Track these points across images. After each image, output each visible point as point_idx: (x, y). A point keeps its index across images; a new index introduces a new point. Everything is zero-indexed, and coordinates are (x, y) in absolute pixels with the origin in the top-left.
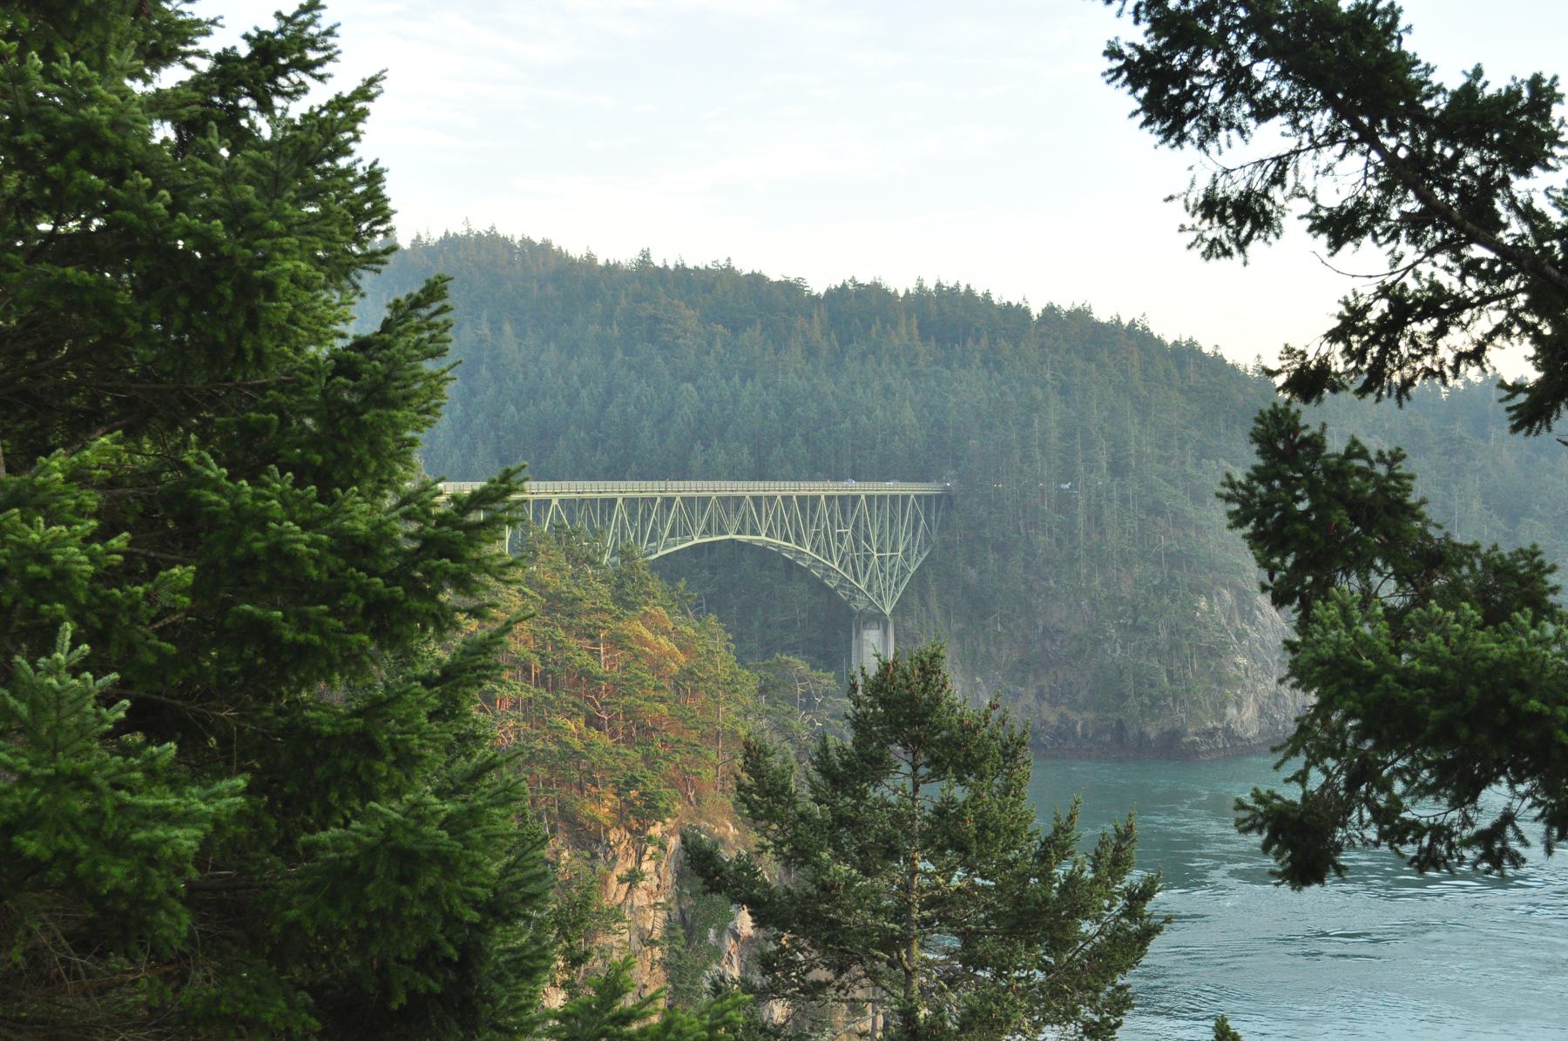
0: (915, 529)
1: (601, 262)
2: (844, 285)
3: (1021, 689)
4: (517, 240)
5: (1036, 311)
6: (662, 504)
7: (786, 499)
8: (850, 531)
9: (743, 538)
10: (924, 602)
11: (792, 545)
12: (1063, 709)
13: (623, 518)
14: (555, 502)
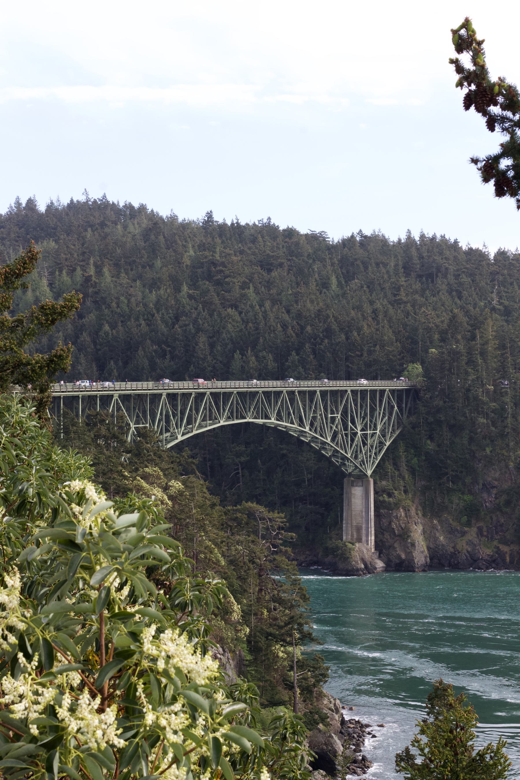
0: (391, 414)
1: (180, 220)
2: (352, 236)
3: (466, 529)
4: (122, 204)
5: (492, 252)
6: (196, 398)
7: (291, 394)
8: (339, 416)
9: (260, 421)
10: (396, 465)
11: (295, 426)
12: (495, 543)
13: (167, 412)
14: (116, 397)
